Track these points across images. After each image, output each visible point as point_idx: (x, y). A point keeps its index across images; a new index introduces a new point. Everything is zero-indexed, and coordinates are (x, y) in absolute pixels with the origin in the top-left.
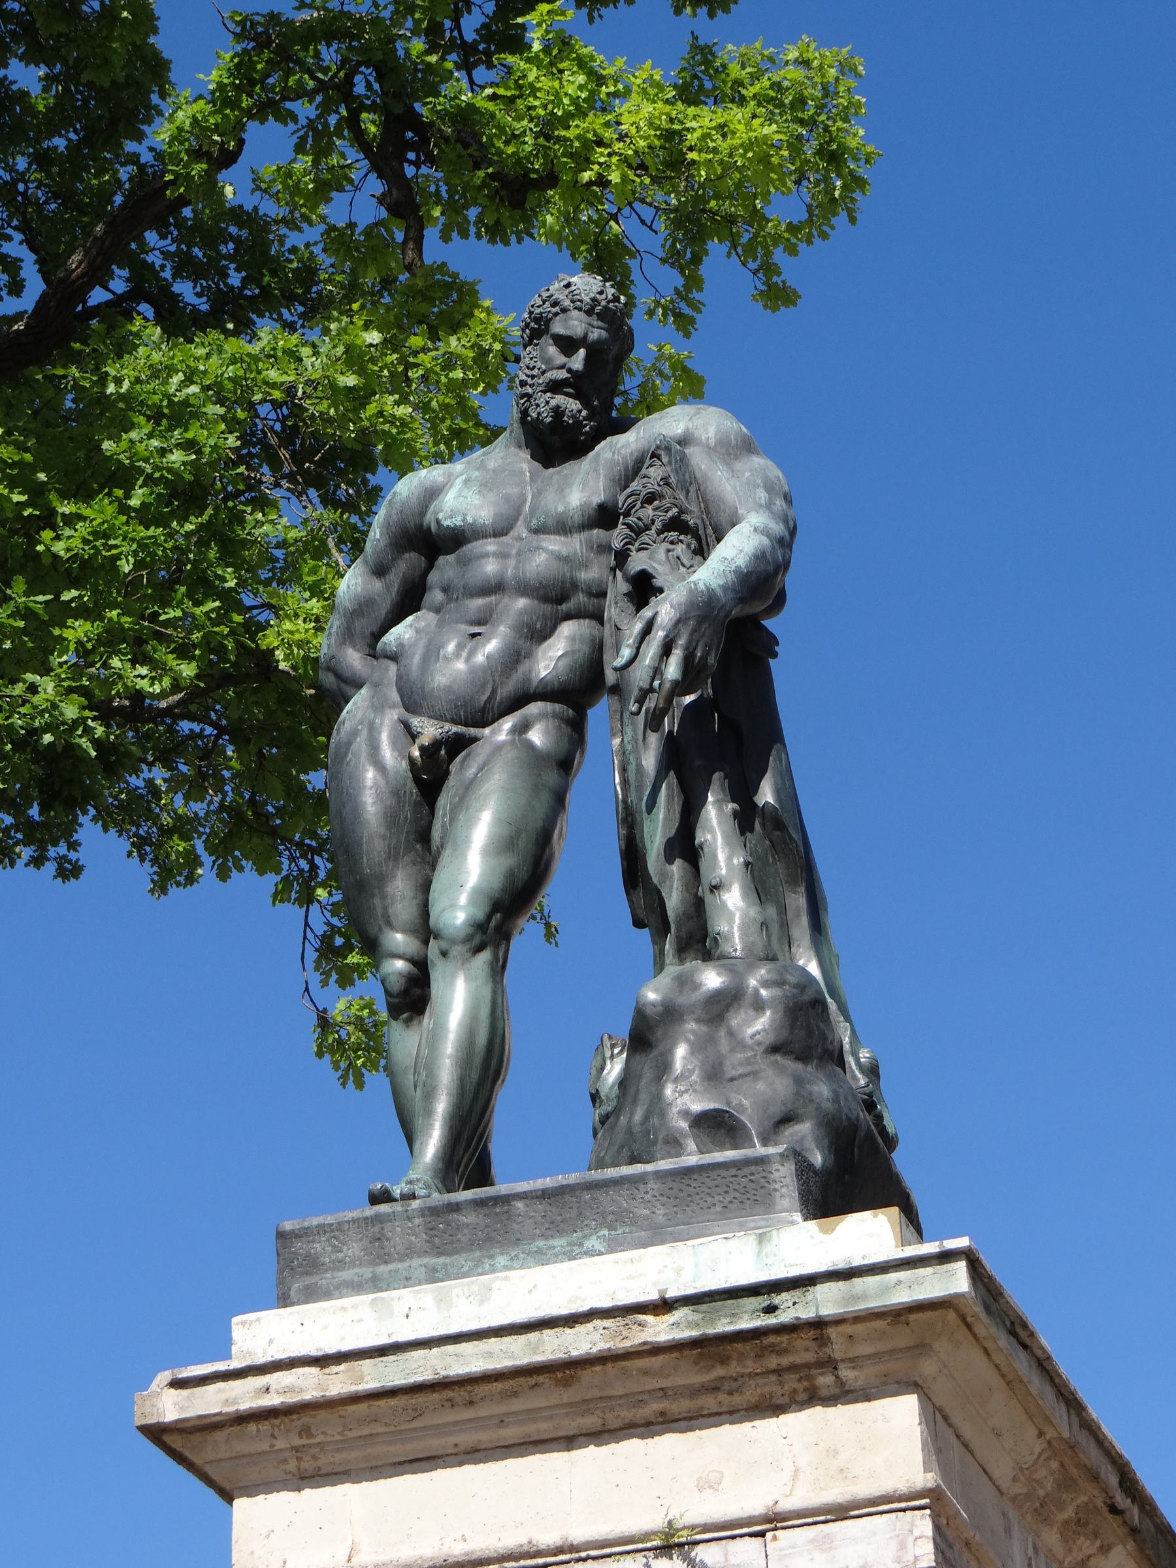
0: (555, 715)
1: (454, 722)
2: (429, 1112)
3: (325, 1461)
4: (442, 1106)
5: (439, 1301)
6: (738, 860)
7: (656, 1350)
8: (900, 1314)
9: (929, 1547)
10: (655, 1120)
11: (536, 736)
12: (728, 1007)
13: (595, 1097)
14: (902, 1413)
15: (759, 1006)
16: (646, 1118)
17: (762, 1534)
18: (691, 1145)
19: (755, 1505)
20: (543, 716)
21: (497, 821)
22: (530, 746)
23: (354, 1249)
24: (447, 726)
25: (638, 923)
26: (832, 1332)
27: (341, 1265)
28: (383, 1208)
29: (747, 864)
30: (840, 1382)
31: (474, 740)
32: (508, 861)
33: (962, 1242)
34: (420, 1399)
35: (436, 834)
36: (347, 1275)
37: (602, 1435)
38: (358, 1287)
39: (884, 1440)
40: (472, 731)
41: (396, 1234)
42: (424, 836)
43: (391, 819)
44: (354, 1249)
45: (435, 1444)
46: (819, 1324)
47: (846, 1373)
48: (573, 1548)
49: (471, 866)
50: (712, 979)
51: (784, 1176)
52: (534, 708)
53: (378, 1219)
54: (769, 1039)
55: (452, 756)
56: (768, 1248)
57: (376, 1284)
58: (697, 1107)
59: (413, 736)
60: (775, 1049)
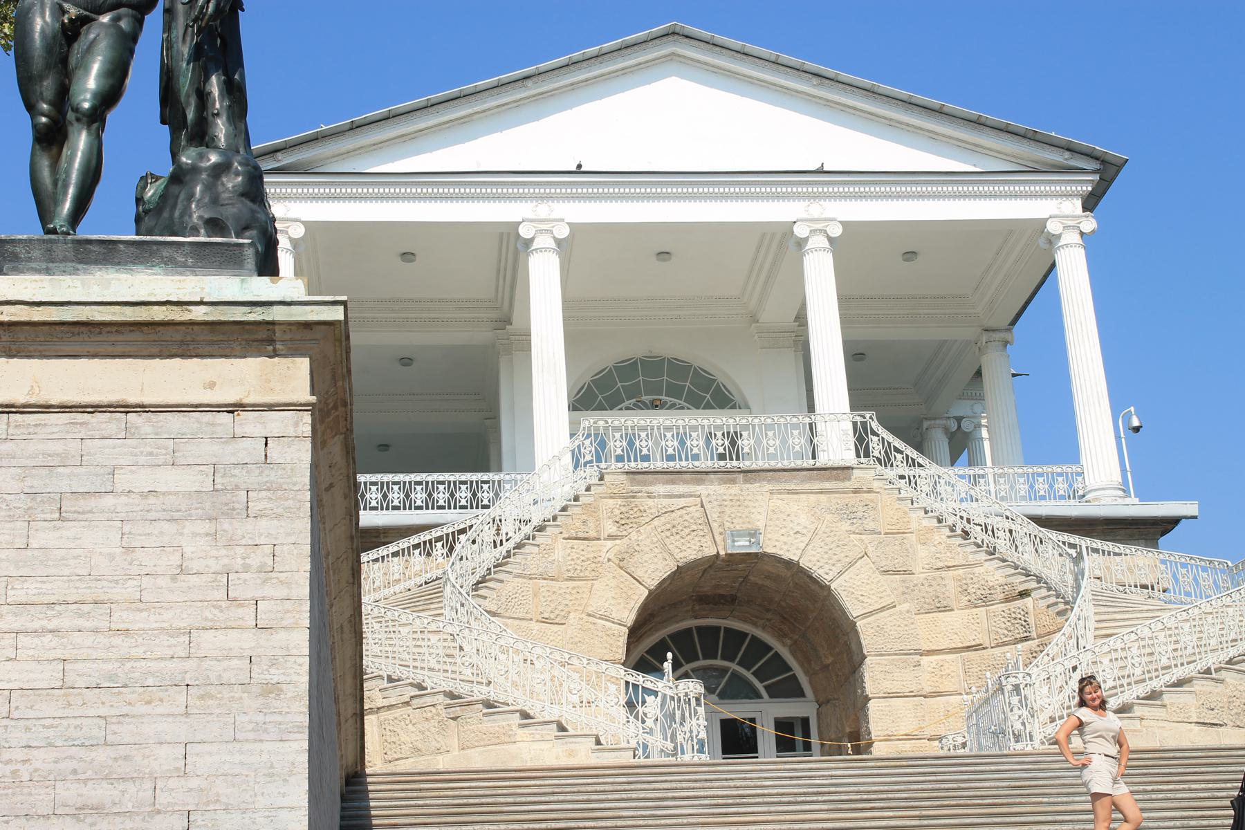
0: (133, 16)
1: (85, 9)
2: (65, 193)
3: (200, 352)
4: (71, 191)
5: (83, 284)
6: (226, 103)
7: (192, 323)
8: (308, 325)
9: (310, 428)
10: (186, 218)
11: (123, 24)
12: (223, 171)
13: (139, 200)
14: (302, 366)
15: (237, 174)
16: (182, 216)
17: (232, 412)
18: (202, 231)
19: (231, 399)
20: (126, 15)
21: (103, 63)
22: (120, 27)
23: (36, 253)
24: (82, 11)
25: (163, 122)
26: (277, 327)
27: (29, 260)
28: (53, 237)
29: (230, 106)
30: (275, 350)
31: (94, 20)
32: (110, 81)
33: (344, 298)
34: (76, 330)
35: (73, 61)
36: (34, 265)
37: (161, 356)
38: (38, 271)
39: (293, 377)
40: (94, 16)
41: (59, 250)
42: (64, 61)
43: (49, 48)
44: (36, 253)
45: (101, 350)
46: (273, 323)
47: (279, 346)
48: (143, 406)
49: (90, 82)
50: (214, 158)
51: (249, 253)
52: (123, 10)
53: (50, 241)
54: (241, 190)
55: (83, 25)
56: (245, 285)
57: (48, 271)
58: (206, 216)
59: (64, 12)
60: (243, 195)
